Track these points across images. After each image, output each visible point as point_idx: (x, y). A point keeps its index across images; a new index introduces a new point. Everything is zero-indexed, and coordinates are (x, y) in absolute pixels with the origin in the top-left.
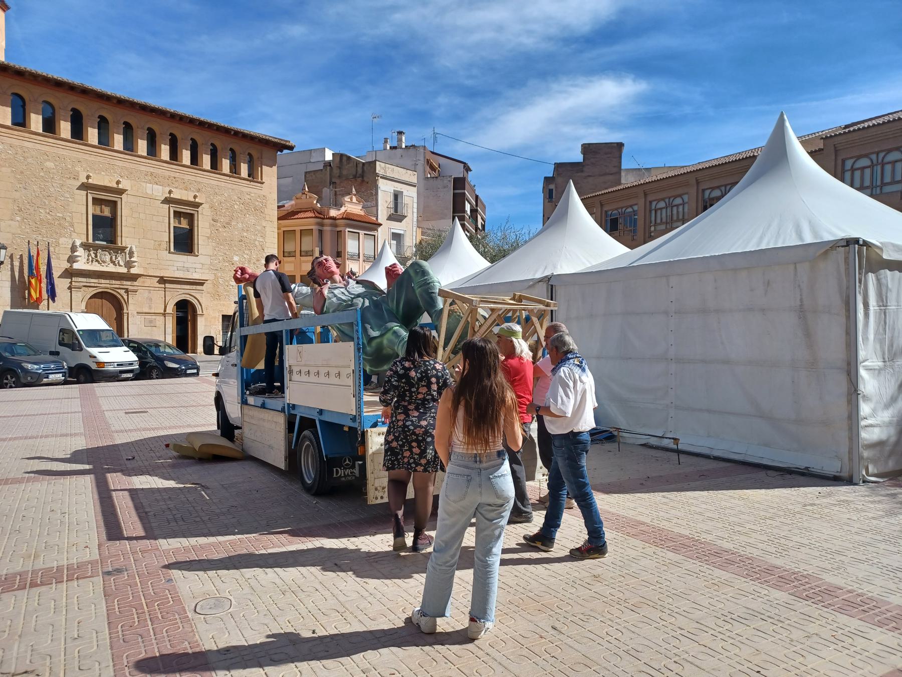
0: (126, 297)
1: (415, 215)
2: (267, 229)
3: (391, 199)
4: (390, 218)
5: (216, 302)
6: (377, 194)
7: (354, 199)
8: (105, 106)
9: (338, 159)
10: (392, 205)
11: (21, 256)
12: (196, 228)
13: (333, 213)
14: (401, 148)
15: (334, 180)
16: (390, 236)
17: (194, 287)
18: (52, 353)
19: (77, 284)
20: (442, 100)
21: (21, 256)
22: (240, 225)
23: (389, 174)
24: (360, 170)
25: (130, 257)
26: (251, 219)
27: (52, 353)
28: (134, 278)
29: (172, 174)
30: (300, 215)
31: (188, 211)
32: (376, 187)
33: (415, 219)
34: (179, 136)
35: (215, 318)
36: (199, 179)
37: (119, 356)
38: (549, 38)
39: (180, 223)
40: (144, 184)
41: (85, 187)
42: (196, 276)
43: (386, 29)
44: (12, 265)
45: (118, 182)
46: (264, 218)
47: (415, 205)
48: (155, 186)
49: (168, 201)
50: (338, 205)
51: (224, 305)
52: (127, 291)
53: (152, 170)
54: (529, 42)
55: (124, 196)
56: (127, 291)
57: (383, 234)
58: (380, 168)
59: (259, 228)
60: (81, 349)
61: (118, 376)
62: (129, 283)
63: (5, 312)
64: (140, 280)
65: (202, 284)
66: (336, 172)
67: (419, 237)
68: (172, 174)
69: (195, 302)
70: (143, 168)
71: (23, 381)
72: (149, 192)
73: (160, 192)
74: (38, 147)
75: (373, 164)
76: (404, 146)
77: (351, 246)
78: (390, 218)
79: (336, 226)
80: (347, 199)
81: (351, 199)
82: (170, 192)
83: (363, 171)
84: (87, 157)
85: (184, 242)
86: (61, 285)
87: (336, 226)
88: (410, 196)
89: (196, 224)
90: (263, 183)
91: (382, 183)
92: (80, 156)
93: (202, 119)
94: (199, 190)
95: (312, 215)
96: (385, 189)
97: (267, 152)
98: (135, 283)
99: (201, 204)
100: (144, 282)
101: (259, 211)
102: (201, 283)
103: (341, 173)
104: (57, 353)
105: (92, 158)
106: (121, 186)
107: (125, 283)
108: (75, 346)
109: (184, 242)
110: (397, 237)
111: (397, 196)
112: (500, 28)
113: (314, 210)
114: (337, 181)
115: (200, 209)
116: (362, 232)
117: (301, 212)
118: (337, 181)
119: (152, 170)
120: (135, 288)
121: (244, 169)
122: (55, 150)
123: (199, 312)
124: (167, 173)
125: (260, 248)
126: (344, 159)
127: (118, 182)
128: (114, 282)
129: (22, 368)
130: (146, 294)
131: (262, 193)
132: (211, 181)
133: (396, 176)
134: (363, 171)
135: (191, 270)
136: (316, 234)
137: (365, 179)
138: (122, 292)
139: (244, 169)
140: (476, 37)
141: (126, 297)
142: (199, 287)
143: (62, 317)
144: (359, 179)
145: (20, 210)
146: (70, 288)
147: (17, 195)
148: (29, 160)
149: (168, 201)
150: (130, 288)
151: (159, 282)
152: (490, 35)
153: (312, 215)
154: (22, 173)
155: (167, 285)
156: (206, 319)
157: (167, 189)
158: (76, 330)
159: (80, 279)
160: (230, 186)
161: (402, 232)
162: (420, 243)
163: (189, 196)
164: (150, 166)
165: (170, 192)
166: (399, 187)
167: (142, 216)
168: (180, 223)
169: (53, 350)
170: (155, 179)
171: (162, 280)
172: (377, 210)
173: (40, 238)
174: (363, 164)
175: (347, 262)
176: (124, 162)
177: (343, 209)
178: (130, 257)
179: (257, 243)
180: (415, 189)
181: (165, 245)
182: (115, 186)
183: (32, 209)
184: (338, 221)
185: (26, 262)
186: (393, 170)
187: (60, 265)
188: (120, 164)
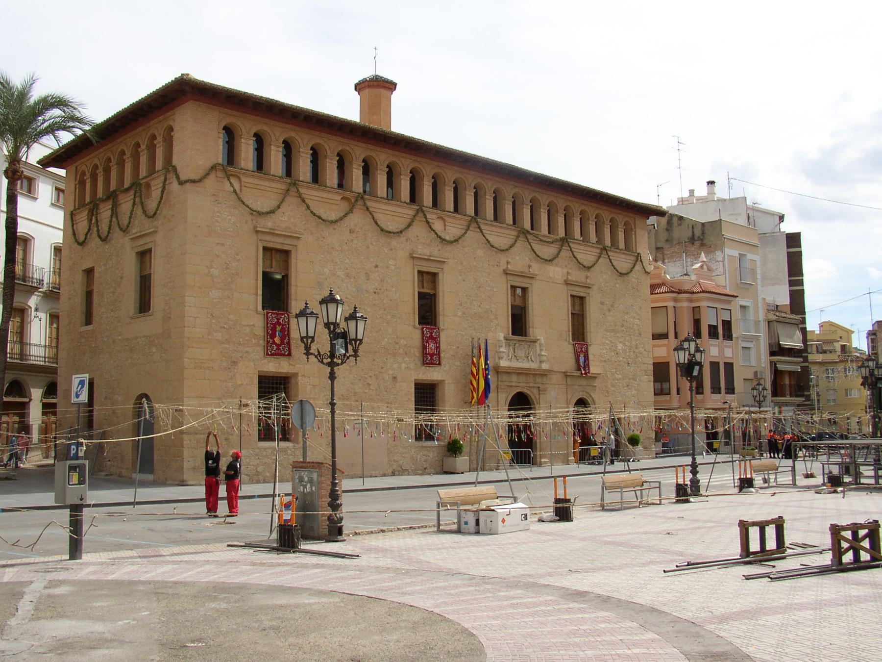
15: (659, 245)
24: (698, 233)
28: (544, 374)
126: (675, 219)
137: (705, 242)
138: (535, 391)
157: (565, 270)
174: (703, 224)
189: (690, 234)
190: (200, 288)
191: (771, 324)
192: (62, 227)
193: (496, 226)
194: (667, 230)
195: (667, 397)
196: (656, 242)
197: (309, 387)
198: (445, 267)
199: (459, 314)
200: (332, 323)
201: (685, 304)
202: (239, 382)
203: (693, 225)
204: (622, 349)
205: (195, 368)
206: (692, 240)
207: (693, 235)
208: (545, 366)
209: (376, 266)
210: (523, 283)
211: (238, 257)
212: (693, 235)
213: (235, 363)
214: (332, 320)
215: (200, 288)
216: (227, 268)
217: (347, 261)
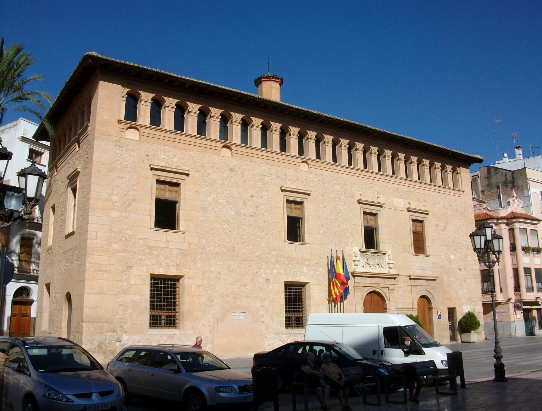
24: (509, 178)
48: (400, 200)
73: (401, 203)
83: (513, 178)
85: (419, 245)
109: (419, 245)
126: (493, 170)
134: (513, 178)
157: (407, 202)
163: (419, 206)
174: (513, 172)
190: (102, 209)
197: (194, 287)
200: (497, 252)
202: (133, 282)
205: (95, 270)
209: (252, 196)
211: (135, 187)
213: (130, 268)
215: (102, 209)
216: (125, 195)
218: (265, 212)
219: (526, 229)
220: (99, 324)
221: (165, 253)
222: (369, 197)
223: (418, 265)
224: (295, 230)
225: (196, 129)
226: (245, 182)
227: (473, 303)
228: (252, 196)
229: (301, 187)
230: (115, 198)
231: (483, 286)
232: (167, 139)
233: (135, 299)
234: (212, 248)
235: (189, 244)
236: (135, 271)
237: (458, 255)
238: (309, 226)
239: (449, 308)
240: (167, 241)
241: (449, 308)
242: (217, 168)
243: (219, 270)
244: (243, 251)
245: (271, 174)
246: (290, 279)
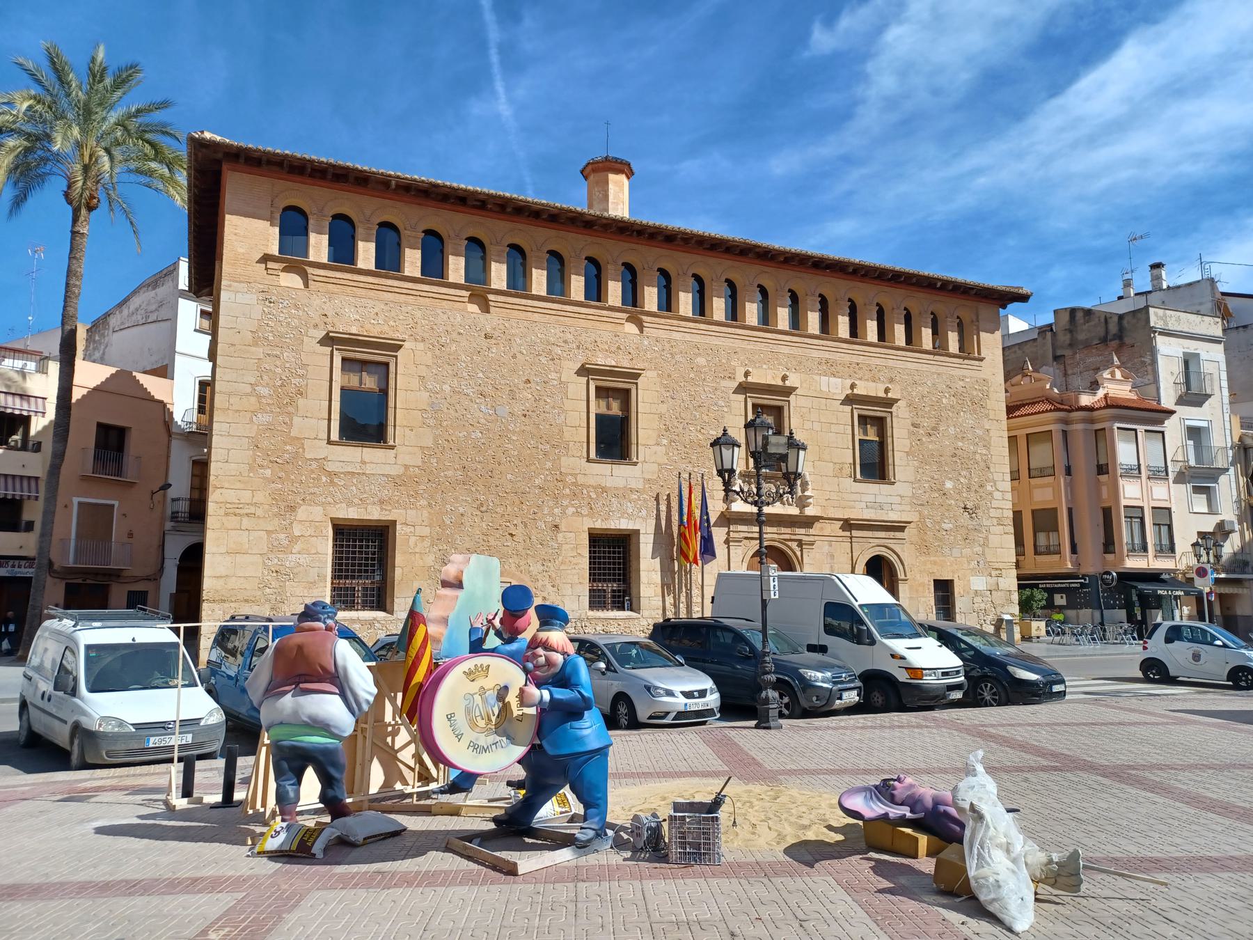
0: (799, 553)
1: (1226, 392)
2: (992, 433)
3: (1178, 368)
4: (1181, 401)
5: (923, 558)
6: (1154, 362)
7: (1118, 375)
8: (766, 269)
9: (1066, 318)
10: (1181, 379)
11: (669, 495)
12: (890, 440)
13: (1085, 400)
14: (1161, 289)
15: (1059, 353)
16: (1184, 432)
17: (891, 534)
18: (812, 648)
19: (736, 535)
20: (1058, 273)
21: (669, 495)
22: (952, 430)
23: (1173, 326)
24: (1113, 328)
25: (803, 491)
26: (967, 420)
27: (812, 648)
28: (809, 522)
29: (855, 359)
30: (1023, 411)
31: (879, 414)
32: (1153, 352)
33: (1226, 400)
34: (859, 302)
35: (923, 585)
36: (891, 363)
37: (931, 658)
38: (1234, 157)
39: (866, 433)
40: (817, 378)
41: (743, 388)
42: (893, 516)
43: (964, 201)
44: (658, 510)
45: (784, 378)
46: (987, 416)
47: (1224, 376)
48: (833, 380)
49: (850, 400)
50: (1094, 386)
51: (935, 563)
52: (800, 544)
53: (827, 355)
54: (1193, 170)
55: (792, 398)
56: (800, 544)
57: (1173, 428)
58: (1156, 317)
59: (979, 432)
60: (873, 642)
61: (944, 697)
62: (802, 531)
63: (720, 575)
64: (817, 525)
65: (902, 529)
66: (1064, 338)
67: (1238, 432)
68: (855, 359)
69: (893, 558)
70: (815, 354)
71: (804, 703)
72: (825, 389)
73: (838, 387)
74: (688, 337)
75: (1141, 314)
76: (1165, 287)
77: (1125, 453)
78: (1181, 401)
79: (1092, 421)
80: (1106, 374)
81: (1113, 374)
82: (853, 386)
83: (1121, 328)
84: (744, 345)
85: (875, 465)
86: (719, 535)
87: (1092, 421)
88: (1213, 358)
89: (889, 434)
90: (981, 360)
91: (1162, 343)
92: (738, 344)
93: (897, 268)
94: (891, 380)
95: (1049, 407)
96: (1169, 352)
97: (985, 310)
98: (812, 531)
99: (896, 401)
100: (822, 529)
101: (978, 405)
102: (901, 528)
103: (1072, 339)
104: (823, 649)
105: (751, 346)
106: (788, 383)
107: (799, 531)
108: (860, 637)
109: (875, 465)
110: (1195, 433)
111: (1189, 361)
112: (1143, 162)
113: (1049, 400)
114: (1067, 353)
115: (894, 409)
116: (1141, 428)
117: (1024, 405)
118: (1067, 353)
119: (827, 355)
120: (811, 538)
121: (953, 339)
122: (709, 340)
123: (901, 575)
124: (847, 358)
125: (982, 464)
126: (1079, 315)
127: (784, 378)
128: (783, 530)
129: (802, 679)
130: (826, 548)
131: (982, 375)
132: (907, 364)
133: (1185, 328)
134: (1121, 328)
135: (885, 507)
136: (1057, 438)
137: (1127, 340)
138: (794, 545)
139: (953, 339)
140: (1104, 182)
141: (799, 553)
142: (898, 535)
143: (826, 581)
144: (1115, 343)
145: (667, 430)
146: (727, 542)
147: (663, 408)
148: (678, 357)
149: (850, 400)
150: (805, 538)
151: (843, 528)
152: (1125, 174)
153: (1049, 407)
154: (669, 376)
155: (855, 533)
156: (911, 588)
157: (848, 382)
158: (856, 604)
159: (741, 528)
160: (934, 369)
161: (1204, 424)
162: (1240, 439)
163: (876, 390)
164: (820, 351)
165: (853, 386)
166: (1192, 346)
167: (817, 426)
168: (866, 433)
169: (815, 642)
170: (831, 369)
171: (848, 525)
172: (1158, 389)
173: (690, 468)
174: (1121, 317)
175: (1121, 482)
176: (789, 348)
177: (1101, 393)
178: (803, 491)
179: (978, 457)
180: (1221, 347)
181: (848, 470)
182: (780, 383)
183: (681, 426)
184: (1096, 413)
185: (675, 505)
186: (1178, 320)
187: (716, 507)
188: (785, 350)
189: (1102, 334)
191: (383, 368)
192: (177, 357)
193: (553, 301)
194: (1071, 331)
195: (1056, 557)
196: (1054, 350)
197: (413, 539)
198: (640, 381)
199: (665, 442)
200: (727, 471)
201: (1080, 427)
202: (297, 533)
203: (1107, 318)
204: (954, 488)
205: (227, 514)
206: (1104, 340)
207: (1107, 332)
208: (809, 511)
209: (528, 381)
210: (877, 412)
212: (1107, 332)
213: (292, 509)
214: (727, 466)
217: (481, 375)
218: (554, 408)
219: (1135, 430)
220: (233, 605)
221: (364, 483)
222: (761, 376)
223: (869, 500)
224: (614, 439)
225: (419, 264)
226: (514, 357)
227: (994, 573)
228: (528, 381)
229: (624, 363)
230: (264, 391)
231: (209, 453)
232: (362, 285)
233: (301, 562)
234: (450, 473)
235: (406, 467)
236: (302, 513)
237: (962, 480)
238: (645, 430)
239: (100, 425)
240: (363, 462)
241: (100, 425)
242: (460, 334)
243: (461, 510)
244: (509, 476)
245: (565, 342)
246: (599, 525)
